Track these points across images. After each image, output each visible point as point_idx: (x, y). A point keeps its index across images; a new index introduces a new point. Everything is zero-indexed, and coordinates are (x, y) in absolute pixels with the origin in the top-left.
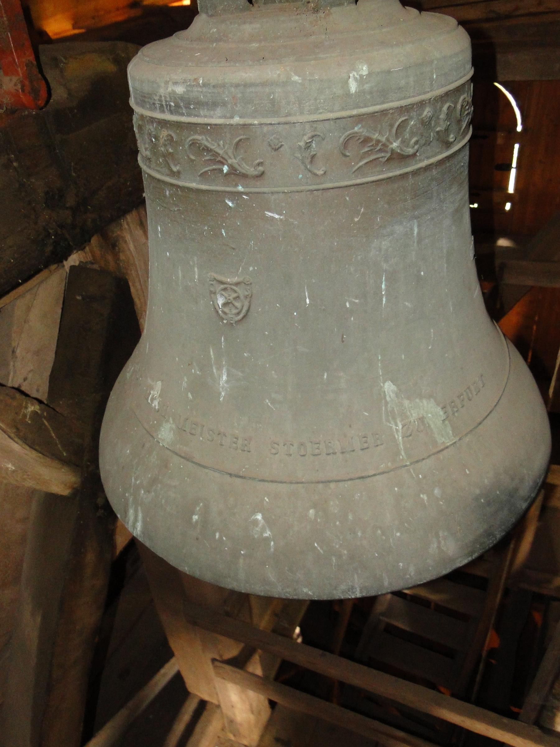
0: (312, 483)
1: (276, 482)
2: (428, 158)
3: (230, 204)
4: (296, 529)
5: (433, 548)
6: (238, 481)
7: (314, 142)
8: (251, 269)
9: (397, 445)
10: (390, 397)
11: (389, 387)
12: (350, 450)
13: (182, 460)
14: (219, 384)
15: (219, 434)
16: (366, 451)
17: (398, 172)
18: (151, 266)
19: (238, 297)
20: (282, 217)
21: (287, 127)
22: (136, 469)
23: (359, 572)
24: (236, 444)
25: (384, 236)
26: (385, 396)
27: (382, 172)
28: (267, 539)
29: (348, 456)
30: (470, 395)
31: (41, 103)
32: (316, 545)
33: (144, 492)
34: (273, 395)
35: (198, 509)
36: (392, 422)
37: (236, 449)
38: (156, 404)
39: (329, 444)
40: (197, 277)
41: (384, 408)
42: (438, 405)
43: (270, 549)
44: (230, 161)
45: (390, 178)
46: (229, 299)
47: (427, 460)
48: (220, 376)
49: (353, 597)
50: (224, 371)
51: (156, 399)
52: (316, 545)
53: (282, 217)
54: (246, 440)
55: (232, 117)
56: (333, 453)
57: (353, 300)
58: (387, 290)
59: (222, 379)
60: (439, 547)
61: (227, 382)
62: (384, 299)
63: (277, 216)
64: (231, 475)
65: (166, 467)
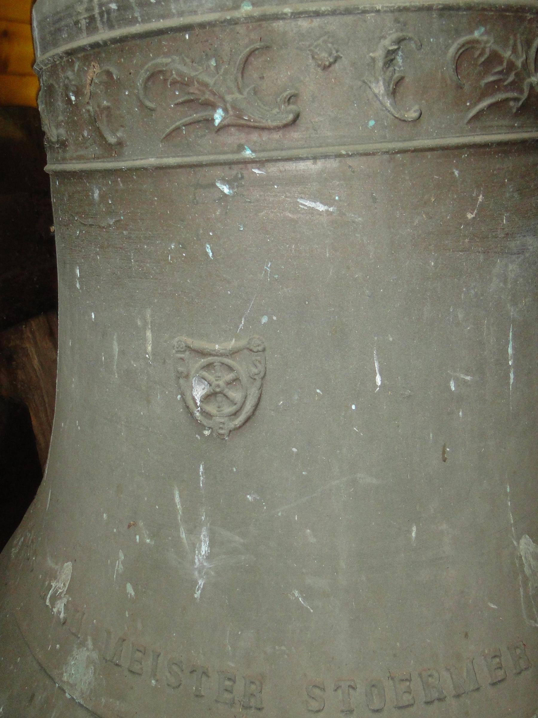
7: (400, 53)
8: (265, 320)
10: (530, 565)
12: (472, 688)
14: (193, 563)
15: (192, 672)
18: (60, 359)
20: (331, 209)
21: (349, 19)
24: (231, 692)
26: (522, 565)
27: (511, 128)
37: (232, 704)
38: (60, 606)
40: (149, 348)
44: (229, 98)
45: (524, 142)
46: (218, 386)
48: (194, 545)
50: (204, 534)
51: (60, 598)
53: (331, 209)
54: (252, 683)
55: (237, 7)
56: (439, 700)
57: (462, 376)
59: (200, 553)
61: (209, 557)
62: (512, 376)
63: (321, 208)
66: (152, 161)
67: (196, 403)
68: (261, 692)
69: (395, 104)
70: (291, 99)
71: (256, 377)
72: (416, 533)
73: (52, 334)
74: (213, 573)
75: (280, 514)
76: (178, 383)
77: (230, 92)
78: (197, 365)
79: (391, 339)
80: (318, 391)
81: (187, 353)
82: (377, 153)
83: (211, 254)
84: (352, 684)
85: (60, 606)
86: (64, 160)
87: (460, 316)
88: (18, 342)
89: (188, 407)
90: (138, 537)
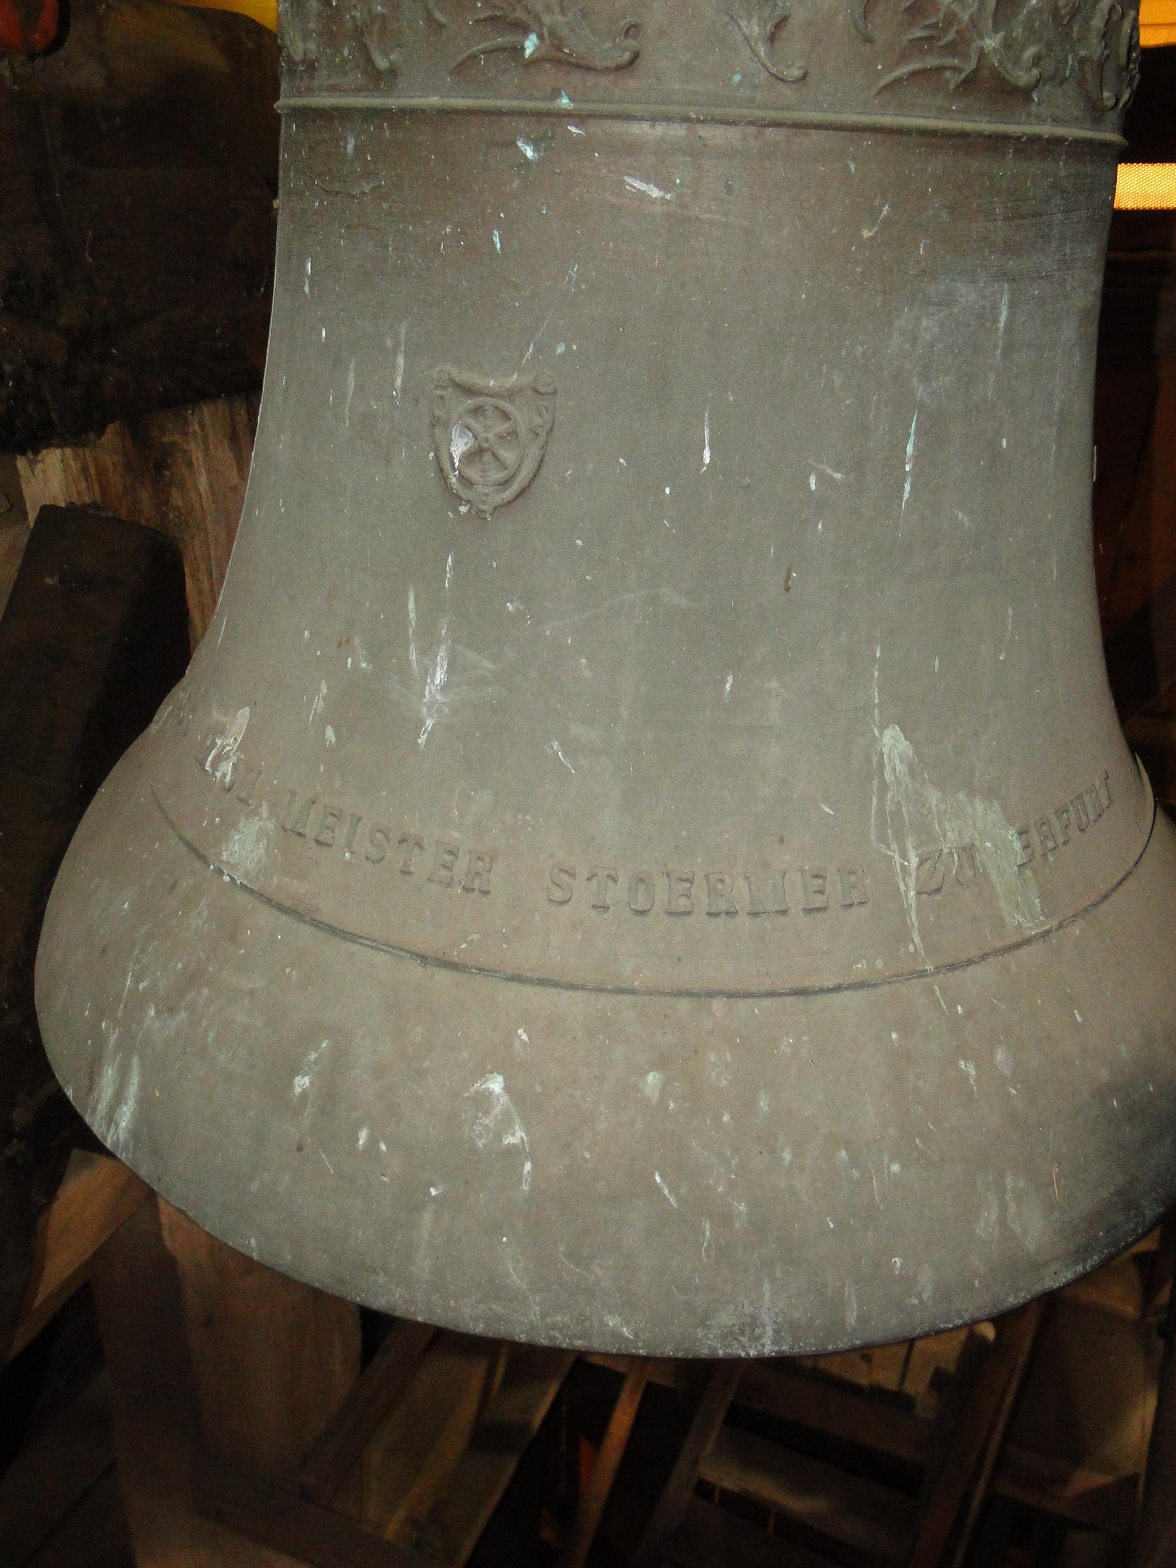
0: (661, 993)
1: (556, 984)
2: (1055, 121)
3: (530, 153)
4: (602, 1126)
5: (987, 1222)
6: (443, 976)
8: (561, 349)
9: (903, 912)
11: (893, 743)
12: (776, 908)
13: (284, 918)
16: (817, 916)
17: (985, 126)
18: (265, 408)
19: (514, 434)
20: (668, 197)
22: (142, 951)
23: (778, 1274)
25: (928, 304)
26: (881, 765)
27: (946, 112)
28: (513, 1155)
29: (767, 924)
30: (1084, 819)
31: (39, 39)
32: (658, 1179)
33: (157, 1012)
34: (575, 729)
35: (313, 1056)
36: (894, 846)
38: (227, 767)
39: (720, 886)
40: (399, 381)
41: (875, 799)
42: (1010, 819)
43: (519, 1181)
44: (546, 19)
45: (963, 135)
46: (487, 440)
47: (978, 967)
48: (426, 671)
49: (753, 1353)
51: (228, 758)
52: (658, 1179)
53: (668, 197)
54: (480, 859)
56: (728, 913)
57: (829, 471)
58: (916, 458)
60: (1002, 1222)
61: (445, 688)
62: (907, 487)
63: (655, 193)
64: (423, 959)
65: (232, 938)
66: (434, 101)
67: (453, 464)
68: (489, 870)
69: (771, 52)
70: (632, 30)
71: (539, 431)
72: (732, 686)
73: (241, 436)
74: (447, 710)
75: (548, 633)
76: (432, 435)
77: (549, 10)
78: (461, 408)
79: (731, 398)
80: (622, 460)
81: (450, 390)
82: (740, 122)
83: (498, 246)
84: (613, 873)
85: (227, 767)
86: (310, 90)
87: (837, 382)
88: (177, 437)
89: (441, 470)
90: (350, 660)
